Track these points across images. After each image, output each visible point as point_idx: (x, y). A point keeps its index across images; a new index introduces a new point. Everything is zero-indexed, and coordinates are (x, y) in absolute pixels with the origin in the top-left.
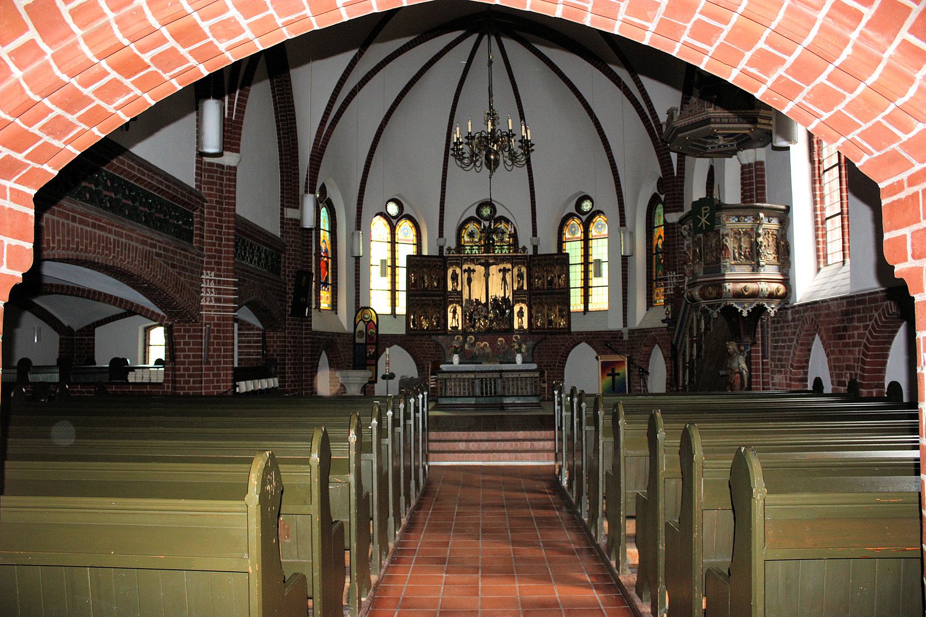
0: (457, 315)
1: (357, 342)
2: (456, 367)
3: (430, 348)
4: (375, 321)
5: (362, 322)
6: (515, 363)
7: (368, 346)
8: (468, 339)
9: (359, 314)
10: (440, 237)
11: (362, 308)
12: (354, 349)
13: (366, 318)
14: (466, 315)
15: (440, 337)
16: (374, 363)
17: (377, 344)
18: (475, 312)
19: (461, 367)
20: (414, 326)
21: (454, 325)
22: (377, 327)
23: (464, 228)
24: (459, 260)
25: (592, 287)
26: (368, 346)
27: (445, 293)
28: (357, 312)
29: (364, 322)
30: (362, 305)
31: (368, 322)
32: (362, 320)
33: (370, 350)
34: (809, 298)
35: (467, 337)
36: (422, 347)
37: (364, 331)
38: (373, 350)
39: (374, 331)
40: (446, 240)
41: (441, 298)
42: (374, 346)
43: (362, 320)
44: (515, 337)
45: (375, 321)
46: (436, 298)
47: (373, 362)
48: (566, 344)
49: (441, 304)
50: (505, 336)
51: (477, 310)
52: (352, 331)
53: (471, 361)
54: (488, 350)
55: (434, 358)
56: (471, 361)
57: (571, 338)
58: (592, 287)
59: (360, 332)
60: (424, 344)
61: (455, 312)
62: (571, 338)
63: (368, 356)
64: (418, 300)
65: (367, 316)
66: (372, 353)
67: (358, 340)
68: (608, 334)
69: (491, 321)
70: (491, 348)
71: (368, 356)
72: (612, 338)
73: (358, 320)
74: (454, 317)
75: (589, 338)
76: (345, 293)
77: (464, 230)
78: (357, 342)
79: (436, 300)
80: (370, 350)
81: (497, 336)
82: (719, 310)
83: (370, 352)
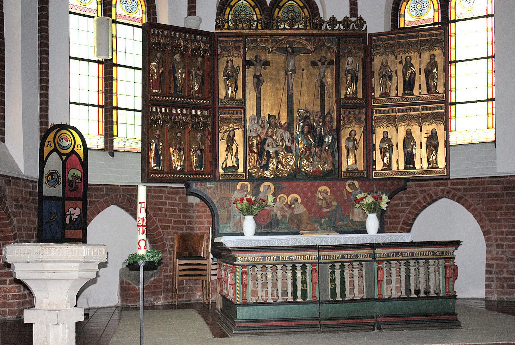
0: (234, 147)
1: (45, 194)
2: (250, 241)
3: (174, 211)
4: (81, 153)
5: (55, 154)
6: (364, 231)
7: (67, 203)
8: (262, 189)
9: (51, 137)
10: (189, 14)
11: (55, 127)
12: (40, 209)
13: (63, 148)
14: (251, 146)
15: (208, 185)
16: (81, 237)
17: (84, 199)
18: (269, 140)
19: (257, 241)
20: (158, 165)
21: (229, 164)
22: (85, 165)
23: (229, 5)
24: (239, 41)
25: (455, 103)
26: (67, 203)
27: (214, 102)
28: (43, 140)
29: (60, 154)
30: (52, 121)
31: (68, 155)
32: (55, 150)
33: (71, 210)
34: (334, 233)
35: (260, 185)
36: (161, 209)
37: (61, 173)
38: (78, 211)
39: (79, 174)
40: (200, 20)
41: (207, 113)
42: (80, 203)
43: (55, 150)
44: (349, 185)
45: (81, 153)
46: (198, 112)
47: (78, 234)
48: (414, 202)
49: (206, 124)
50: (331, 183)
51: (271, 137)
52: (35, 175)
53: (269, 230)
54: (300, 209)
55: (182, 229)
56: (269, 230)
57: (423, 191)
58: (455, 103)
59: (51, 174)
60: (164, 204)
61: (231, 140)
62: (423, 191)
63: (68, 221)
64: (165, 114)
65: (65, 144)
66: (73, 217)
67: (48, 191)
68: (498, 183)
69: (299, 157)
70: (306, 206)
71: (68, 221)
72: (503, 189)
73: (47, 150)
74: (229, 149)
75: (459, 190)
76: (20, 83)
77: (228, 9)
78: (45, 194)
79: (198, 116)
80: (71, 210)
81: (316, 183)
82: (211, 256)
83: (71, 215)
